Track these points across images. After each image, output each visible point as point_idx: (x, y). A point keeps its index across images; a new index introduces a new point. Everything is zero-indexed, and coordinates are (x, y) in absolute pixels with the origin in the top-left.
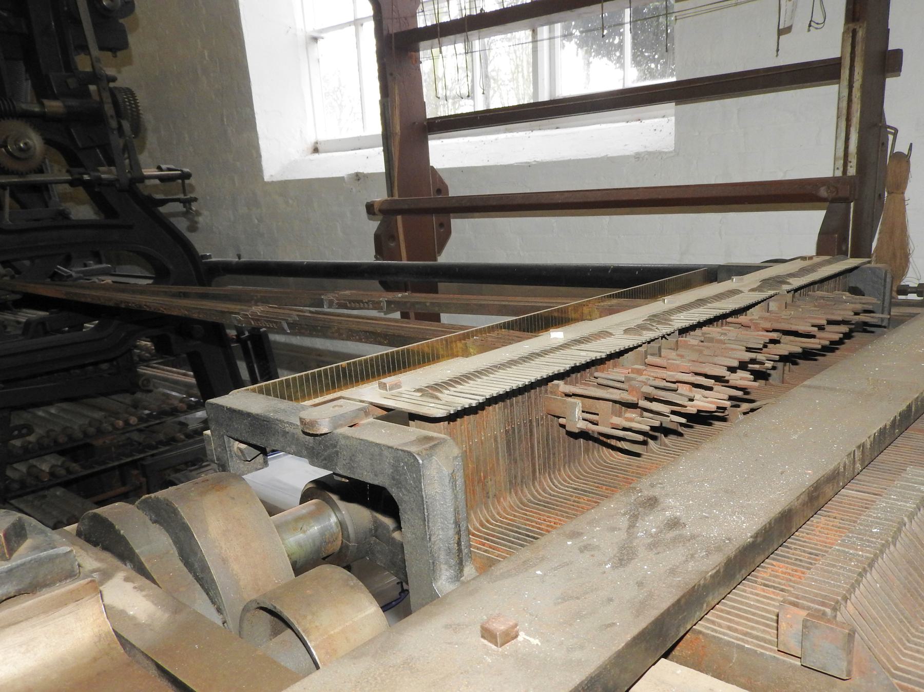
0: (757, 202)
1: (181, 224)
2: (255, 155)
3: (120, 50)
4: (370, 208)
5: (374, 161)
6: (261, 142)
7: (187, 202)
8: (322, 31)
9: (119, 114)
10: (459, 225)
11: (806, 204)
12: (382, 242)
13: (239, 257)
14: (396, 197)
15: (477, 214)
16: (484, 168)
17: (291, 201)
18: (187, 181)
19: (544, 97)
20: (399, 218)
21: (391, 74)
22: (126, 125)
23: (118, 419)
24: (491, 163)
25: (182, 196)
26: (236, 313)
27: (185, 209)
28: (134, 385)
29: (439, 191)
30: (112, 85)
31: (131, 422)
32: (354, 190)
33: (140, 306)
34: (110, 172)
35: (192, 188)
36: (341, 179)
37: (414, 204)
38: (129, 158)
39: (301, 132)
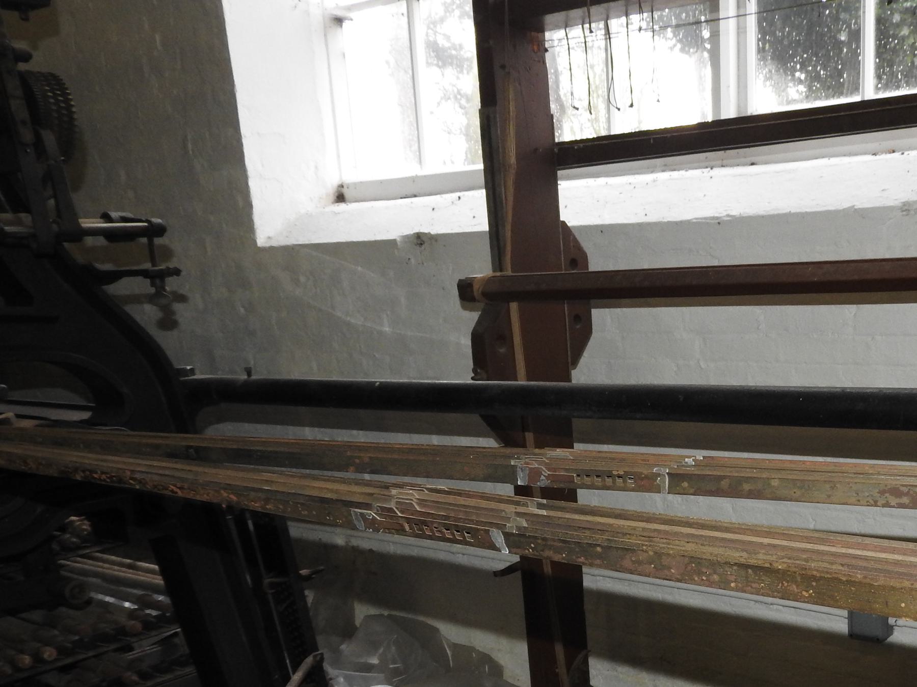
0: (695, 294)
1: (146, 315)
2: (241, 204)
3: (34, 7)
4: (466, 290)
5: (470, 213)
6: (251, 183)
7: (157, 277)
8: (350, 8)
9: (37, 119)
10: (605, 319)
11: (676, 299)
12: (486, 347)
13: (249, 372)
14: (509, 272)
15: (627, 301)
16: (640, 226)
17: (302, 279)
18: (158, 241)
19: (729, 112)
20: (514, 306)
21: (503, 67)
22: (49, 139)
23: (22, 652)
24: (652, 218)
25: (147, 266)
26: (359, 505)
27: (153, 290)
28: (58, 595)
29: (574, 263)
30: (22, 66)
31: (46, 656)
32: (413, 261)
33: (120, 481)
34: (19, 223)
35: (168, 253)
36: (392, 243)
37: (536, 282)
38: (55, 196)
39: (316, 167)
